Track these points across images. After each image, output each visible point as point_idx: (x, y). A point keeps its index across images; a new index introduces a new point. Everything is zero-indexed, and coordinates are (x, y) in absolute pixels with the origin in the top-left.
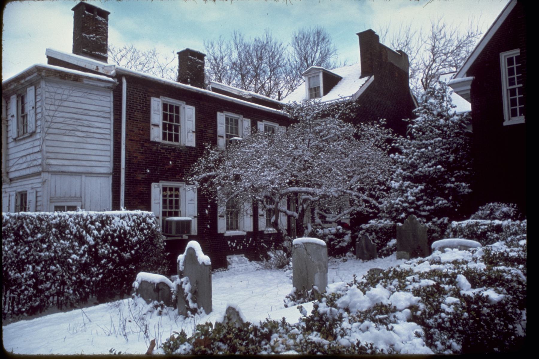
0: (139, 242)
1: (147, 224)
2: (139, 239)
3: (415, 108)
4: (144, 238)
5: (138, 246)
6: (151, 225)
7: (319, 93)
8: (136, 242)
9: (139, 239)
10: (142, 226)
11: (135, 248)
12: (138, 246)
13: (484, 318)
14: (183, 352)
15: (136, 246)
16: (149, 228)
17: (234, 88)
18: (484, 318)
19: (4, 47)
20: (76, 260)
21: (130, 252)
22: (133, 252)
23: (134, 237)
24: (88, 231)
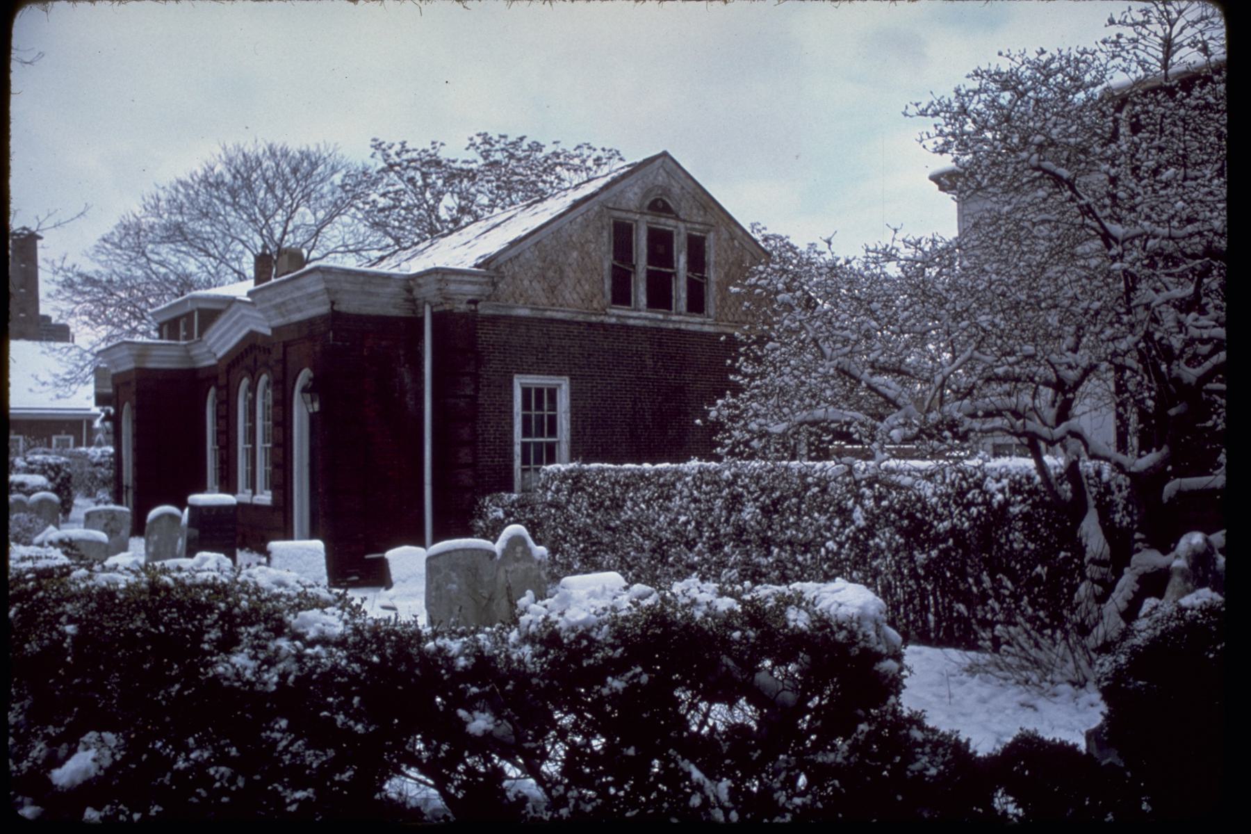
0: (954, 532)
1: (984, 492)
2: (954, 527)
3: (202, 488)
4: (966, 524)
5: (951, 542)
6: (992, 496)
7: (200, 316)
8: (946, 532)
9: (954, 527)
10: (970, 496)
11: (941, 546)
12: (951, 542)
13: (617, 684)
14: (123, 580)
15: (945, 541)
16: (987, 503)
17: (180, 299)
18: (617, 684)
19: (14, 87)
20: (832, 551)
21: (928, 553)
22: (934, 553)
23: (942, 521)
24: (859, 498)
